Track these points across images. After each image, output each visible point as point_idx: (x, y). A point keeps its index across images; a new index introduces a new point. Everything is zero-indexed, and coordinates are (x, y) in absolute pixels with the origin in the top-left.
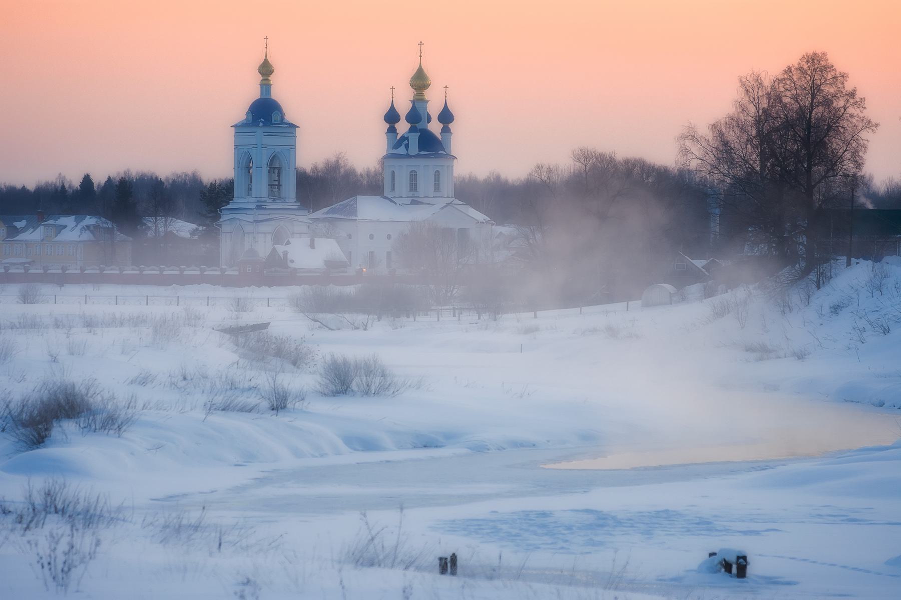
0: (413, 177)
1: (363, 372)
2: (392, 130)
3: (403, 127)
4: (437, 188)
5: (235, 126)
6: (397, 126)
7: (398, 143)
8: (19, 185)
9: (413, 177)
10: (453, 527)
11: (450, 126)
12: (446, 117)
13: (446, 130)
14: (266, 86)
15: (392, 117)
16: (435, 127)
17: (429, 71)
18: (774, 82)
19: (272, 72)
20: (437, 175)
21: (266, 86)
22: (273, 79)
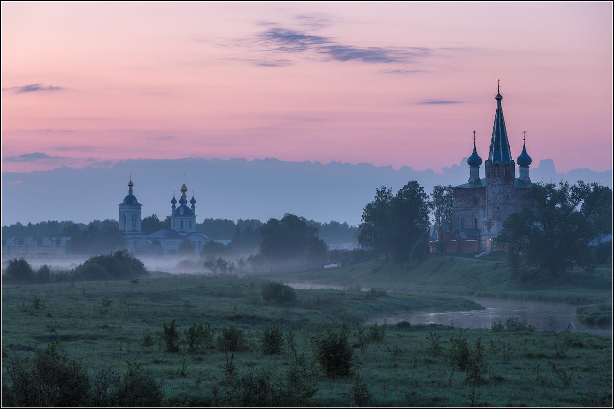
0: (182, 223)
1: (376, 372)
2: (174, 206)
3: (178, 205)
4: (190, 226)
5: (120, 205)
6: (175, 204)
7: (176, 212)
8: (39, 222)
9: (182, 223)
10: (405, 58)
11: (195, 205)
12: (193, 201)
13: (193, 206)
14: (131, 191)
15: (174, 201)
16: (189, 205)
17: (187, 186)
18: (221, 399)
19: (133, 186)
20: (190, 222)
21: (131, 191)
22: (54, 86)
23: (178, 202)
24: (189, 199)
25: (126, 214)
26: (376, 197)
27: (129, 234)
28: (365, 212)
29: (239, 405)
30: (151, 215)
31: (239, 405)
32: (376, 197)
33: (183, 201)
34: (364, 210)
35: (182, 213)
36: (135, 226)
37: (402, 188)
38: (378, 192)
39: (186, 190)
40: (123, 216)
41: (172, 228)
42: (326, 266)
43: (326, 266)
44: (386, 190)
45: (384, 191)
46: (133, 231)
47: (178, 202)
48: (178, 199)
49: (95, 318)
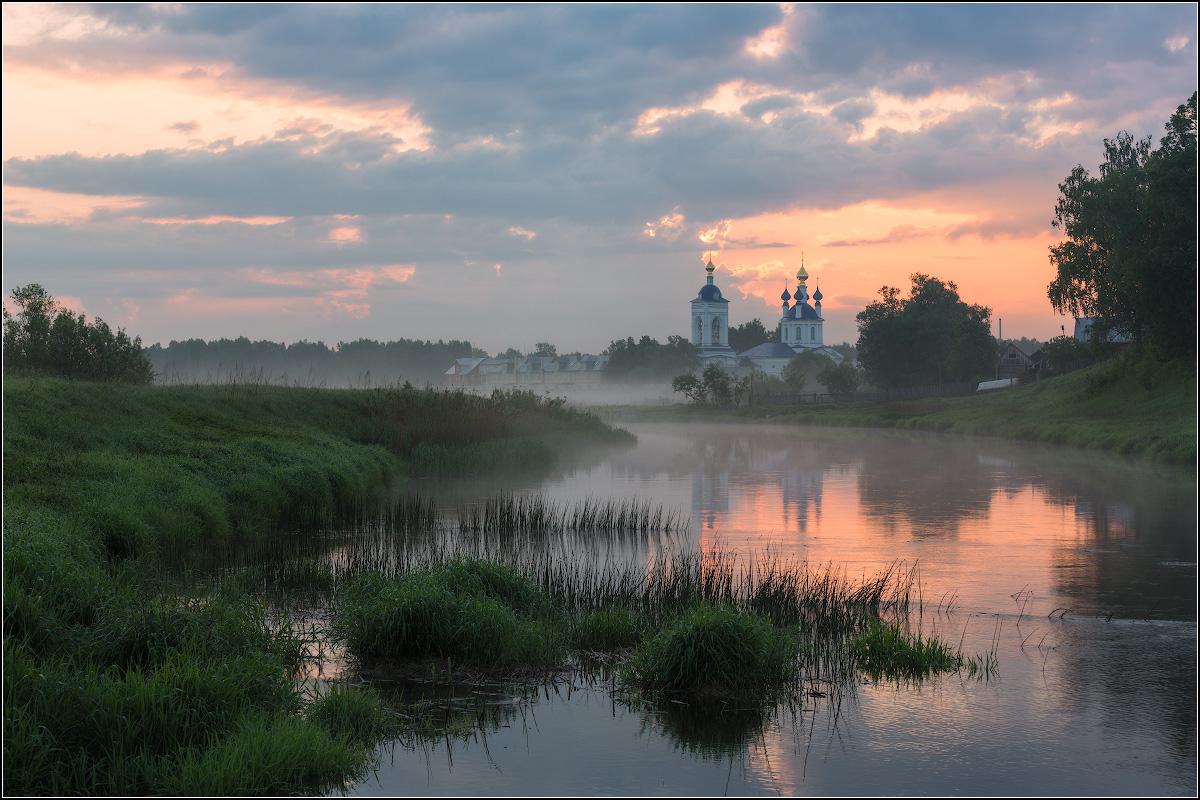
0: (799, 330)
2: (786, 304)
3: (792, 302)
7: (790, 315)
9: (799, 330)
14: (710, 278)
16: (811, 302)
21: (710, 278)
23: (792, 297)
24: (811, 292)
25: (703, 317)
26: (1103, 167)
27: (707, 350)
28: (1064, 197)
29: (7, 715)
30: (751, 320)
31: (7, 710)
32: (1103, 167)
33: (800, 295)
34: (1062, 188)
35: (798, 314)
36: (718, 337)
37: (1186, 104)
38: (1111, 150)
39: (806, 278)
40: (698, 323)
41: (783, 340)
42: (983, 386)
43: (983, 386)
44: (1133, 145)
45: (1128, 146)
46: (714, 344)
47: (792, 297)
48: (792, 292)
49: (214, 440)
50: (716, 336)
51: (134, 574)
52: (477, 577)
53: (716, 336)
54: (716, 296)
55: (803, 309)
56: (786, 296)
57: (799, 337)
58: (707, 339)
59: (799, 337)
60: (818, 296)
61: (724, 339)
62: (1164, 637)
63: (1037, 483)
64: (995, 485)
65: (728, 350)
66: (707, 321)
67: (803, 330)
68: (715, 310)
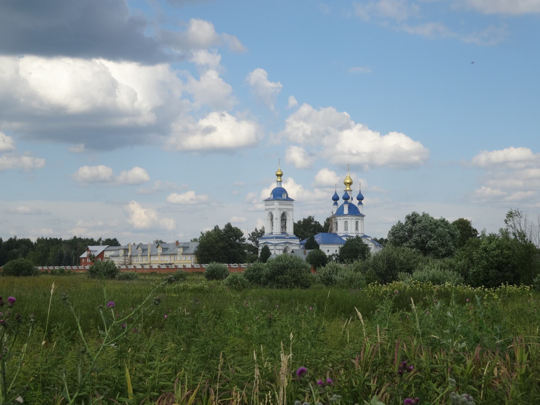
3: (341, 202)
16: (355, 202)
35: (346, 211)
48: (341, 196)
50: (284, 227)
51: (145, 350)
52: (174, 351)
53: (284, 227)
54: (284, 197)
55: (349, 207)
56: (336, 199)
57: (346, 229)
58: (277, 230)
59: (346, 229)
60: (360, 198)
61: (290, 230)
62: (451, 303)
63: (393, 131)
64: (313, 236)
65: (293, 238)
66: (277, 215)
67: (349, 221)
68: (285, 207)
